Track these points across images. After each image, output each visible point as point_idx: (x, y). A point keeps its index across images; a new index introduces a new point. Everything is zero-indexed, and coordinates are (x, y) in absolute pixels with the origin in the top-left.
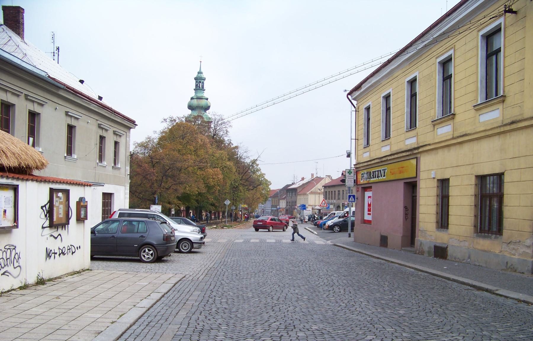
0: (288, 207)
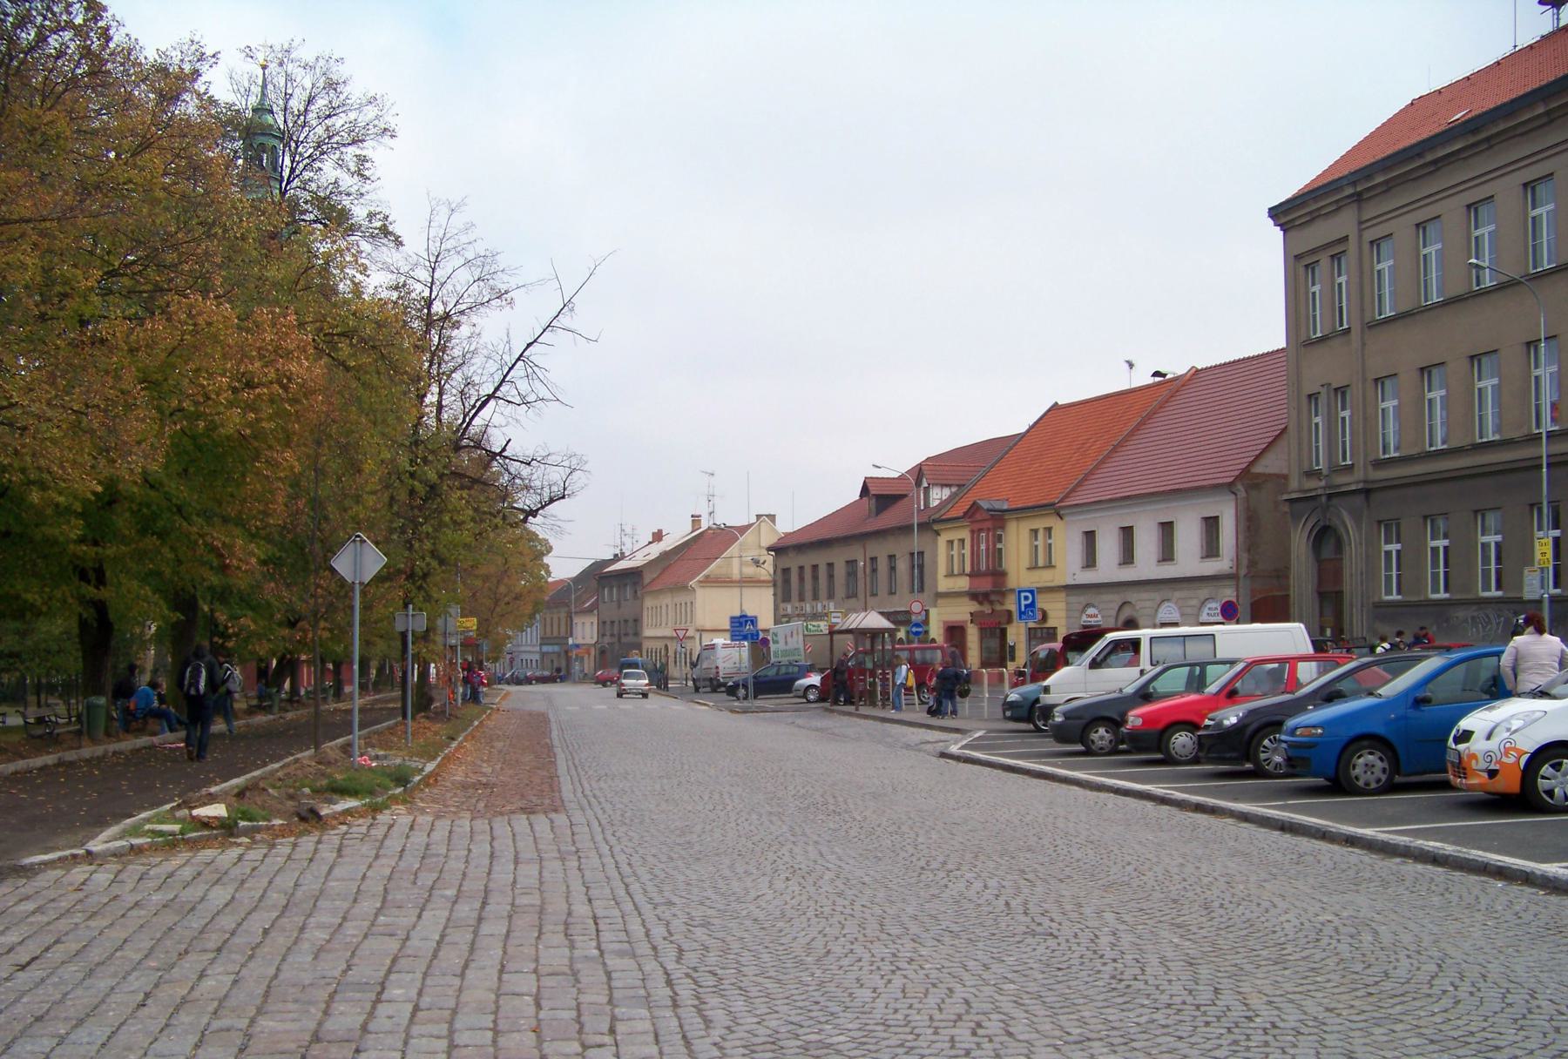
0: (607, 639)
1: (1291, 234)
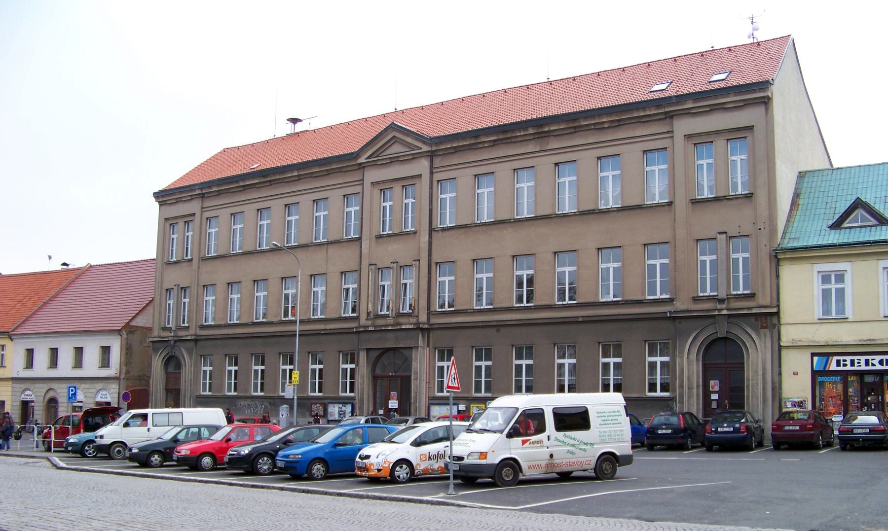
1: (163, 207)
